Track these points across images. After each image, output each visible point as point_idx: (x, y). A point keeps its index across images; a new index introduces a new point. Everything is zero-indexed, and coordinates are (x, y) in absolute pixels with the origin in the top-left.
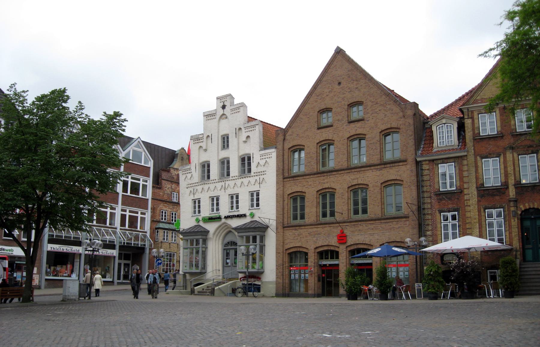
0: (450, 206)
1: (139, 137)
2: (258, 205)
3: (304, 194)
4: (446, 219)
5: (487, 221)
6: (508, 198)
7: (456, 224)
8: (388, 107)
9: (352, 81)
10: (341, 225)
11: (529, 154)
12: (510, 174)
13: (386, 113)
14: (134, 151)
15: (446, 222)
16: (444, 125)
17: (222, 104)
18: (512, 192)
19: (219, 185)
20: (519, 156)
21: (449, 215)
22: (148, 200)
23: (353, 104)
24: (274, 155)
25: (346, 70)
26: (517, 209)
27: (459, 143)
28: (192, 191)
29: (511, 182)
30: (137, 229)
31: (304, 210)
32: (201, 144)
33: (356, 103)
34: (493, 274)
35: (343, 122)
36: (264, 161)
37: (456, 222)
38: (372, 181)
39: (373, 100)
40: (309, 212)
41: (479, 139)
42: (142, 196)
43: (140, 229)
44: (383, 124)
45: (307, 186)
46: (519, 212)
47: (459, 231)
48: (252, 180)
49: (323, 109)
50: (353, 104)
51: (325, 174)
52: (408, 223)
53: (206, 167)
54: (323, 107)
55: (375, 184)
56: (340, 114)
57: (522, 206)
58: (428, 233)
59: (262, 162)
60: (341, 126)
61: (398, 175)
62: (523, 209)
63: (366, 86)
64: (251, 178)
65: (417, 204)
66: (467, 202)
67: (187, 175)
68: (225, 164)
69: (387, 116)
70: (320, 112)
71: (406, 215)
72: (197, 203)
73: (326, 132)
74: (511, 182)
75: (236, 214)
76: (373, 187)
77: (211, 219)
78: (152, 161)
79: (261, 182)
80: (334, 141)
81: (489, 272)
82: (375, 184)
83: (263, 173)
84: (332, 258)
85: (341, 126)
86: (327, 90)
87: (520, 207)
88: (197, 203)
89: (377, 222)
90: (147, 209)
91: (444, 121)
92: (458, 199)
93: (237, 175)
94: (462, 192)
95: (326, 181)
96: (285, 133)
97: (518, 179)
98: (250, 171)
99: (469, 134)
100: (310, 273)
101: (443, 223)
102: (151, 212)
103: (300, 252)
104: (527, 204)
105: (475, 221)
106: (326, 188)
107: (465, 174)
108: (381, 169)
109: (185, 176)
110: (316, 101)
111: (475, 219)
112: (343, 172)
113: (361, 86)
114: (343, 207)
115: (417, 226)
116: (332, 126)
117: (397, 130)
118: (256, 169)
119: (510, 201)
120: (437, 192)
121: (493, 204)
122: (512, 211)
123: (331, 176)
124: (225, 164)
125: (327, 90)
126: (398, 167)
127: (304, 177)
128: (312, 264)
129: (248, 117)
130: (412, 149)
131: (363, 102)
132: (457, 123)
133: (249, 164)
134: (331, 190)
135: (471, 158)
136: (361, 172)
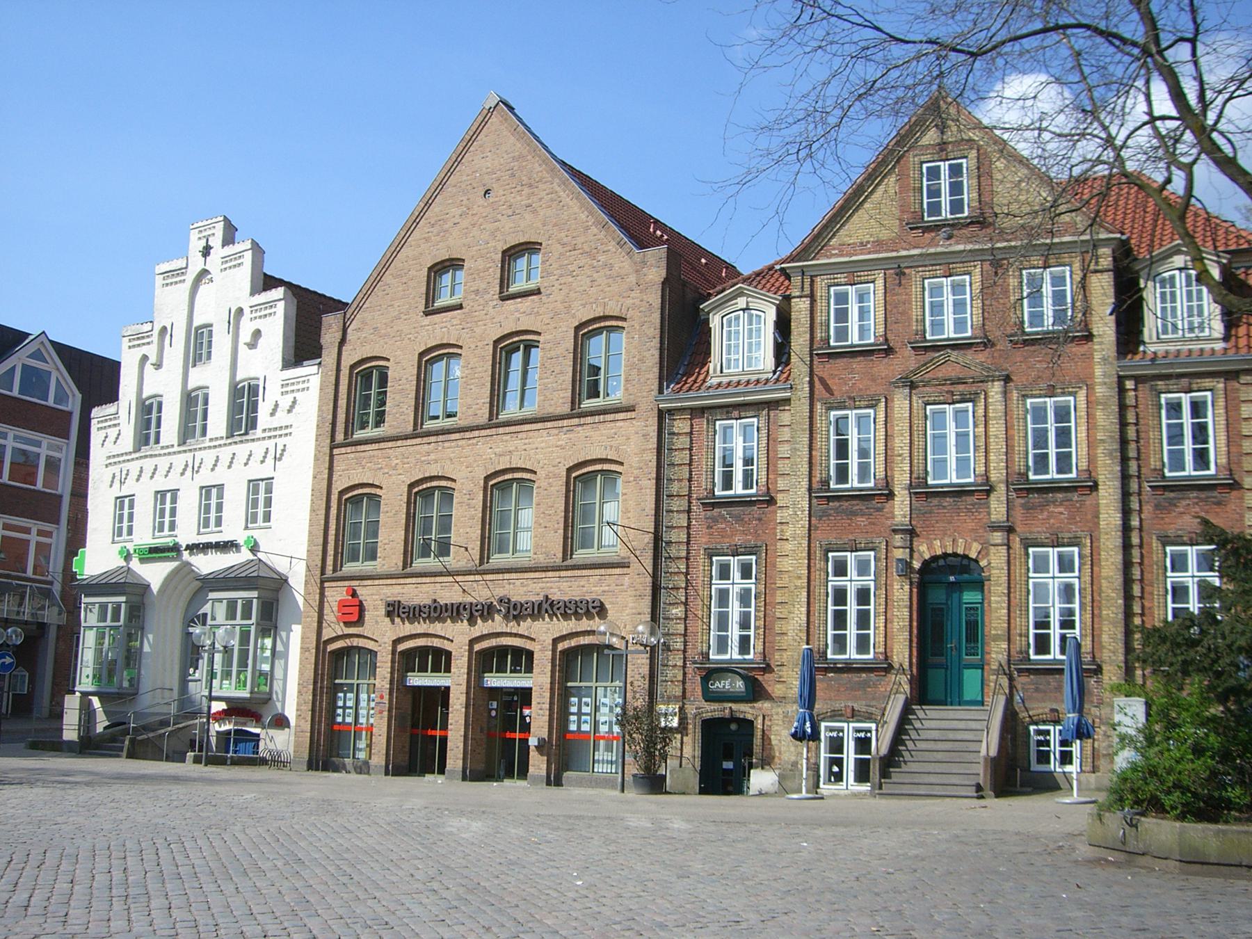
0: (738, 540)
1: (44, 332)
2: (267, 517)
3: (378, 492)
4: (725, 573)
5: (830, 584)
6: (889, 522)
7: (750, 590)
8: (602, 258)
9: (519, 188)
10: (459, 578)
11: (953, 403)
12: (900, 455)
13: (595, 275)
14: (25, 368)
15: (724, 584)
16: (741, 312)
17: (203, 243)
18: (901, 508)
19: (179, 461)
20: (929, 407)
21: (734, 562)
22: (61, 496)
23: (517, 249)
24: (315, 382)
25: (506, 157)
26: (911, 557)
27: (777, 367)
28: (118, 474)
29: (901, 479)
30: (25, 572)
31: (376, 535)
32: (144, 350)
33: (524, 247)
34: (835, 734)
35: (487, 297)
36: (290, 398)
37: (750, 584)
38: (546, 462)
39: (565, 240)
40: (387, 541)
41: (822, 353)
42: (44, 486)
43: (35, 573)
44: (584, 306)
45: (386, 471)
46: (917, 565)
47: (756, 610)
48: (258, 449)
49: (443, 261)
50: (517, 249)
51: (433, 439)
52: (626, 579)
53: (148, 413)
54: (444, 255)
55: (552, 469)
56: (481, 274)
57: (923, 548)
58: (674, 611)
59: (285, 402)
60: (481, 307)
61: (611, 446)
62: (927, 556)
63: (552, 200)
64: (256, 443)
65: (652, 530)
66: (782, 531)
67: (109, 431)
68: (193, 403)
69: (596, 283)
70: (435, 269)
71: (624, 558)
72: (124, 505)
73: (444, 325)
74: (901, 479)
75: (213, 539)
76: (547, 477)
77: (155, 553)
78: (79, 396)
79: (278, 456)
80: (461, 347)
81: (826, 727)
82: (552, 469)
83: (284, 431)
84: (436, 669)
85: (481, 307)
86: (456, 211)
87: (919, 550)
88: (124, 505)
89: (550, 574)
90: (57, 522)
91: (741, 302)
92: (760, 520)
93: (224, 435)
94: (771, 501)
95: (432, 457)
96: (345, 324)
97: (918, 470)
98: (252, 424)
99: (799, 341)
100: (379, 708)
101: (717, 584)
102: (68, 530)
103: (359, 649)
104: (938, 543)
105: (798, 583)
106: (432, 478)
107: (784, 450)
108: (570, 429)
109: (102, 434)
110: (427, 240)
111: (800, 578)
112: (476, 433)
113: (541, 199)
114: (468, 530)
115: (649, 591)
116: (460, 307)
117: (620, 324)
118: (269, 418)
119: (895, 531)
120: (707, 498)
121: (851, 537)
122: (899, 560)
123: (446, 444)
124: (193, 403)
125: (456, 211)
126: (612, 424)
127: (382, 445)
128: (384, 683)
129: (265, 274)
130: (651, 376)
131: (541, 244)
132: (775, 308)
133: (253, 407)
134: (443, 483)
135: (801, 406)
136: (520, 435)
